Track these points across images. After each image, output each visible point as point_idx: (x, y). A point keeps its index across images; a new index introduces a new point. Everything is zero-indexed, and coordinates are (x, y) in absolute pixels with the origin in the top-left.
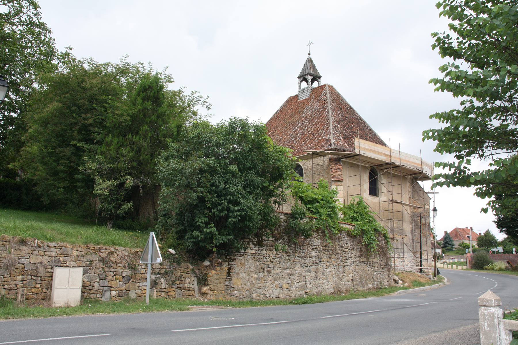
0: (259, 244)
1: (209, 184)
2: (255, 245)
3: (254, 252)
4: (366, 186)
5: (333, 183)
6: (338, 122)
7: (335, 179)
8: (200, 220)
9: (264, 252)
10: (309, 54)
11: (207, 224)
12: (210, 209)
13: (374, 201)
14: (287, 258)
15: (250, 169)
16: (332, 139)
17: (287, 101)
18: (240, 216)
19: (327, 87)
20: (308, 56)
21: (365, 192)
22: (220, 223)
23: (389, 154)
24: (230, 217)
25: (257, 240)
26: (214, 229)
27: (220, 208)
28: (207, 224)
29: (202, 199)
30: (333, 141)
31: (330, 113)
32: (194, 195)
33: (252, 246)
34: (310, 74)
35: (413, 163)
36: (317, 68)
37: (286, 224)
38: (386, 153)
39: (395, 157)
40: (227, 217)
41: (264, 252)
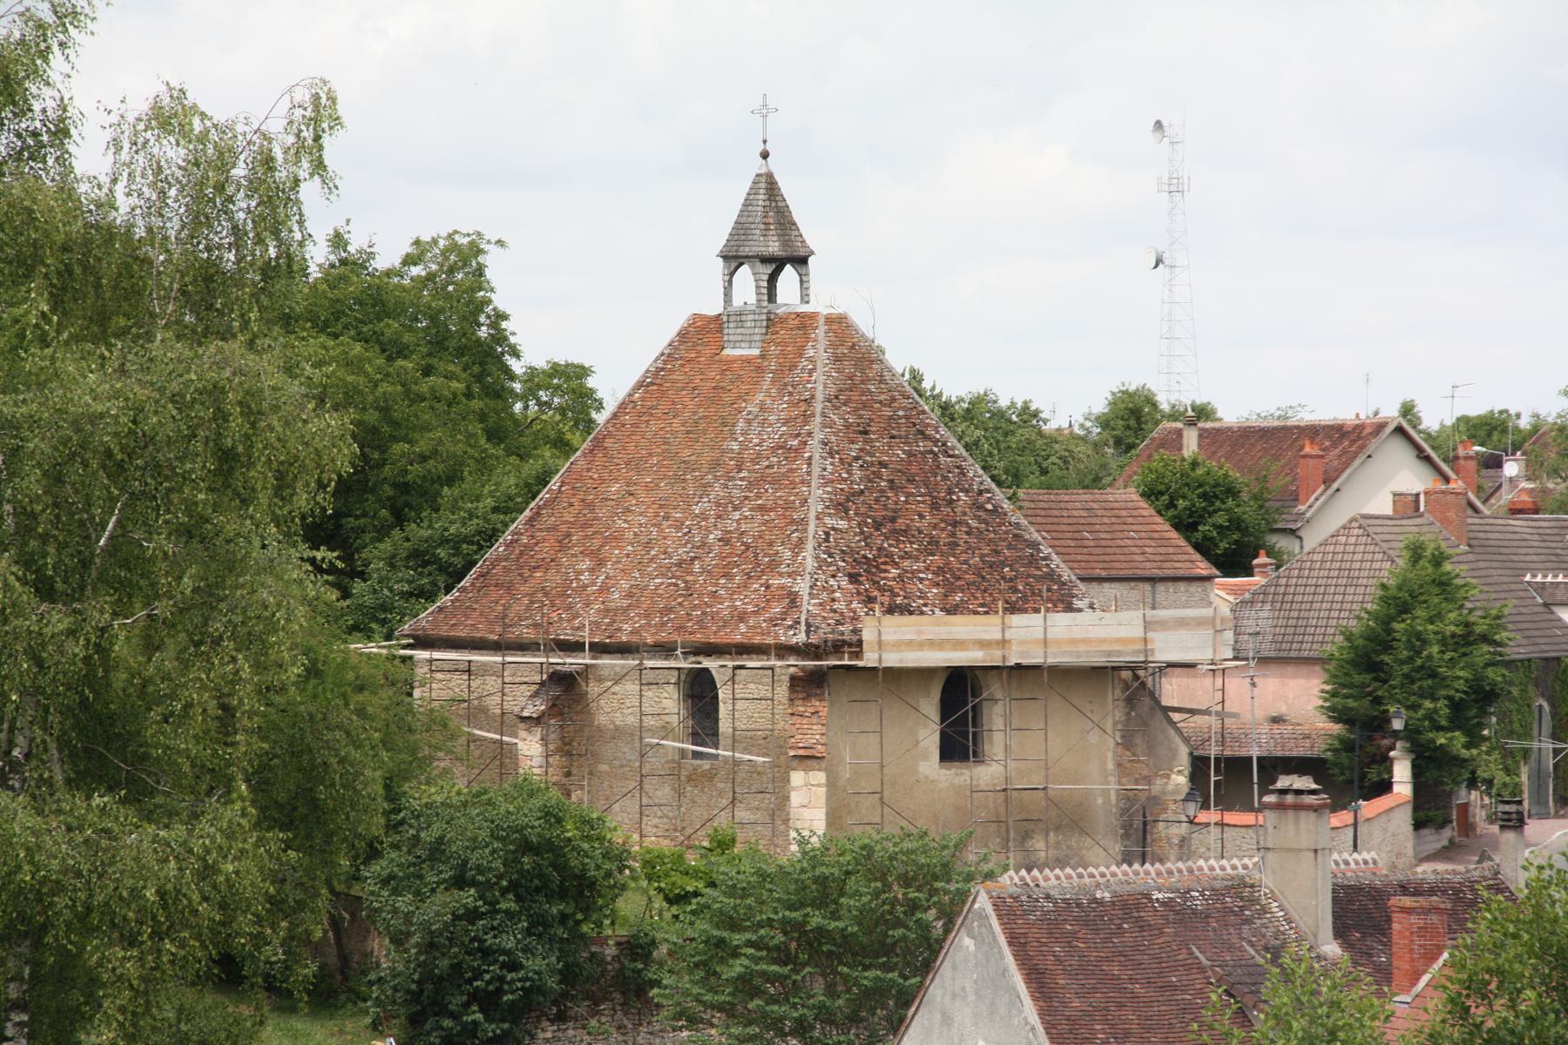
0: (561, 1018)
1: (467, 940)
2: (552, 1022)
3: (549, 1035)
4: (930, 738)
5: (795, 763)
6: (841, 508)
7: (801, 752)
8: (456, 1001)
9: (571, 1033)
10: (765, 155)
11: (467, 1005)
12: (470, 981)
13: (957, 781)
14: (620, 1038)
15: (538, 890)
16: (806, 597)
17: (683, 335)
18: (522, 989)
19: (819, 350)
20: (758, 166)
21: (925, 757)
22: (488, 1001)
23: (998, 636)
24: (506, 993)
25: (555, 1010)
26: (479, 1016)
27: (487, 977)
28: (467, 1005)
29: (457, 967)
30: (808, 605)
31: (816, 470)
32: (444, 963)
33: (545, 1024)
34: (769, 240)
35: (1103, 641)
36: (797, 216)
37: (617, 965)
38: (986, 636)
39: (1022, 642)
40: (499, 992)
41: (571, 1033)
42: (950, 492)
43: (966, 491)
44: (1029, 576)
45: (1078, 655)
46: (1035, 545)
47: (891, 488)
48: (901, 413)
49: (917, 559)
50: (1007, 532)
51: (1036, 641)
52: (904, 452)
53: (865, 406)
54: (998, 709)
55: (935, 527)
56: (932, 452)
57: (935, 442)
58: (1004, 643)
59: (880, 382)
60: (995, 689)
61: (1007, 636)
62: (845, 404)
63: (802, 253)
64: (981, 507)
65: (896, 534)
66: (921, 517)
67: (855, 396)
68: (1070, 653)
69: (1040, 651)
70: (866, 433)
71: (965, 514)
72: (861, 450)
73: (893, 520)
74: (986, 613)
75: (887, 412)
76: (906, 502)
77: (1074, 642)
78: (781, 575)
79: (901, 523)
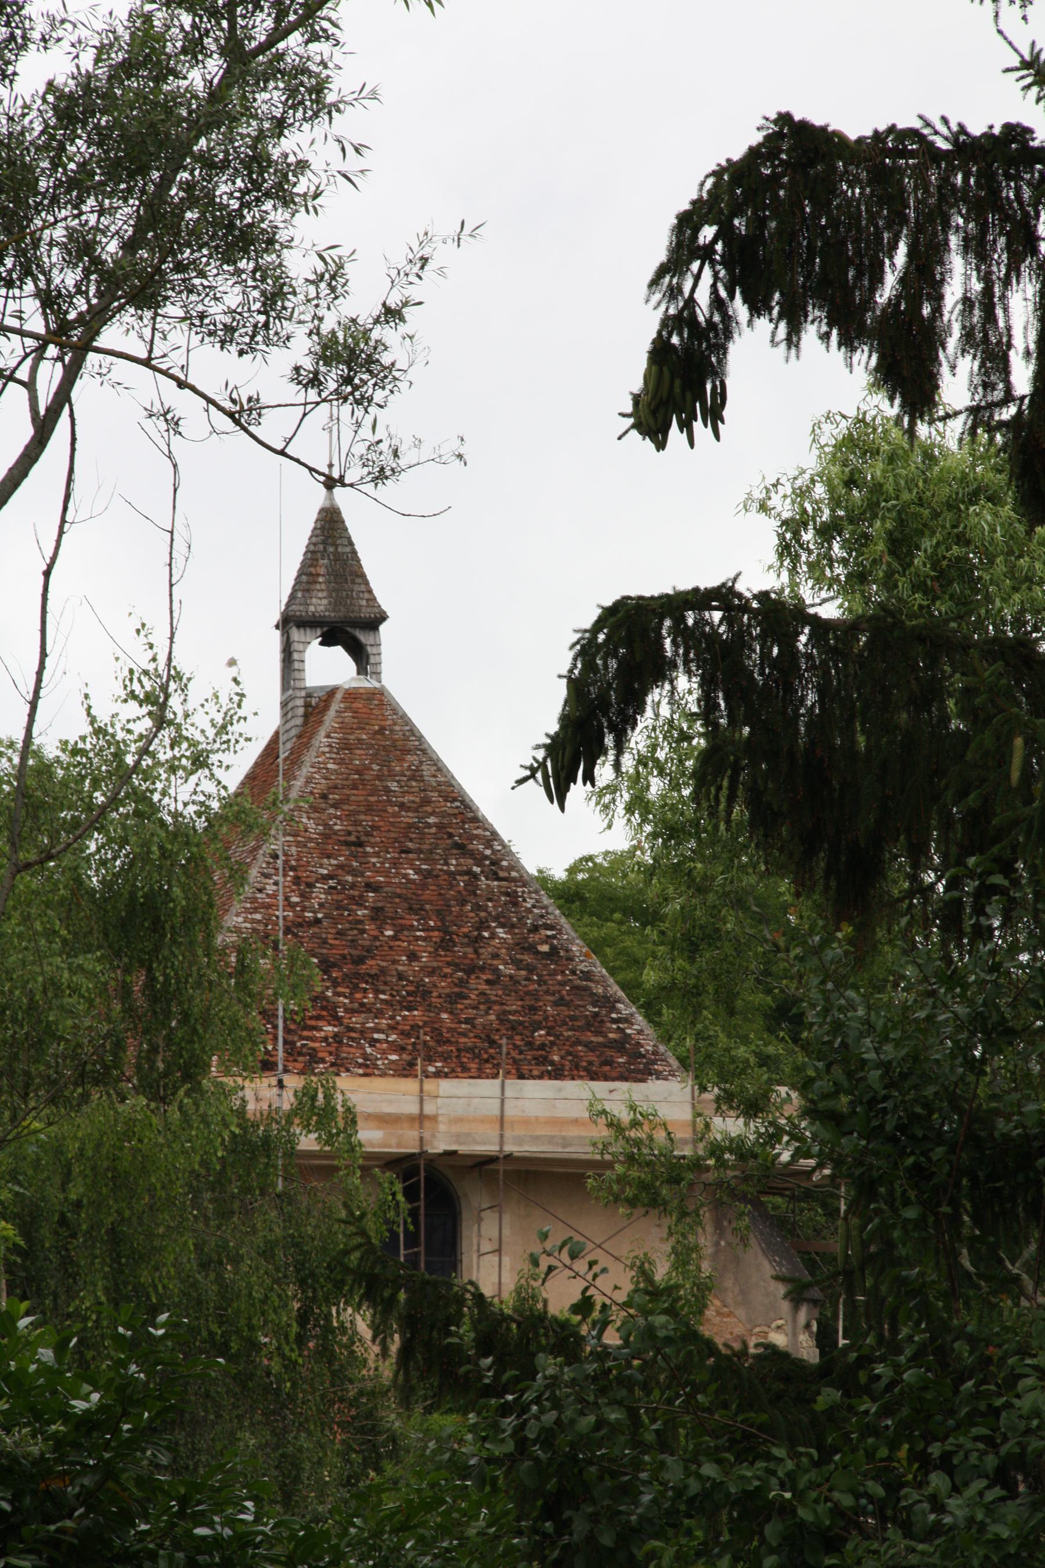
23: (414, 1109)
36: (20, 488)
39: (459, 1120)
42: (482, 925)
43: (510, 927)
44: (578, 1042)
45: (566, 1142)
46: (610, 1003)
47: (373, 919)
48: (431, 820)
49: (379, 1014)
50: (563, 984)
51: (483, 1120)
52: (418, 870)
53: (369, 809)
54: (490, 1226)
55: (432, 972)
56: (469, 872)
57: (479, 859)
58: (421, 1119)
59: (413, 778)
60: (474, 1198)
61: (429, 1109)
62: (335, 806)
63: (365, 613)
64: (532, 949)
65: (353, 981)
66: (413, 957)
67: (358, 796)
68: (551, 1139)
69: (494, 1133)
70: (360, 844)
71: (495, 956)
72: (340, 867)
73: (360, 960)
74: (365, 1075)
75: (408, 818)
76: (395, 938)
77: (554, 1122)
78: (275, 1049)
79: (371, 965)
